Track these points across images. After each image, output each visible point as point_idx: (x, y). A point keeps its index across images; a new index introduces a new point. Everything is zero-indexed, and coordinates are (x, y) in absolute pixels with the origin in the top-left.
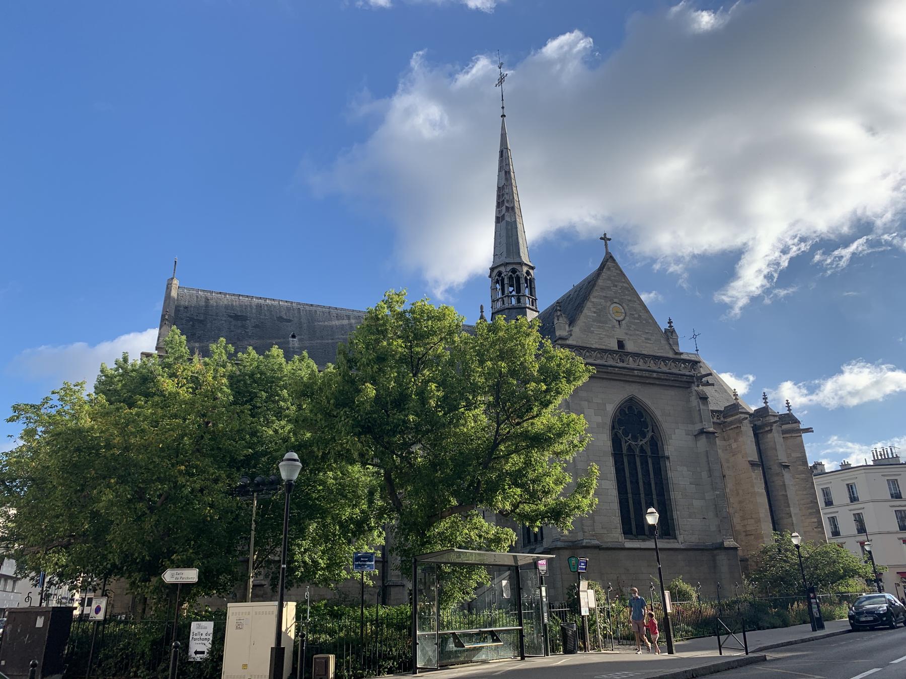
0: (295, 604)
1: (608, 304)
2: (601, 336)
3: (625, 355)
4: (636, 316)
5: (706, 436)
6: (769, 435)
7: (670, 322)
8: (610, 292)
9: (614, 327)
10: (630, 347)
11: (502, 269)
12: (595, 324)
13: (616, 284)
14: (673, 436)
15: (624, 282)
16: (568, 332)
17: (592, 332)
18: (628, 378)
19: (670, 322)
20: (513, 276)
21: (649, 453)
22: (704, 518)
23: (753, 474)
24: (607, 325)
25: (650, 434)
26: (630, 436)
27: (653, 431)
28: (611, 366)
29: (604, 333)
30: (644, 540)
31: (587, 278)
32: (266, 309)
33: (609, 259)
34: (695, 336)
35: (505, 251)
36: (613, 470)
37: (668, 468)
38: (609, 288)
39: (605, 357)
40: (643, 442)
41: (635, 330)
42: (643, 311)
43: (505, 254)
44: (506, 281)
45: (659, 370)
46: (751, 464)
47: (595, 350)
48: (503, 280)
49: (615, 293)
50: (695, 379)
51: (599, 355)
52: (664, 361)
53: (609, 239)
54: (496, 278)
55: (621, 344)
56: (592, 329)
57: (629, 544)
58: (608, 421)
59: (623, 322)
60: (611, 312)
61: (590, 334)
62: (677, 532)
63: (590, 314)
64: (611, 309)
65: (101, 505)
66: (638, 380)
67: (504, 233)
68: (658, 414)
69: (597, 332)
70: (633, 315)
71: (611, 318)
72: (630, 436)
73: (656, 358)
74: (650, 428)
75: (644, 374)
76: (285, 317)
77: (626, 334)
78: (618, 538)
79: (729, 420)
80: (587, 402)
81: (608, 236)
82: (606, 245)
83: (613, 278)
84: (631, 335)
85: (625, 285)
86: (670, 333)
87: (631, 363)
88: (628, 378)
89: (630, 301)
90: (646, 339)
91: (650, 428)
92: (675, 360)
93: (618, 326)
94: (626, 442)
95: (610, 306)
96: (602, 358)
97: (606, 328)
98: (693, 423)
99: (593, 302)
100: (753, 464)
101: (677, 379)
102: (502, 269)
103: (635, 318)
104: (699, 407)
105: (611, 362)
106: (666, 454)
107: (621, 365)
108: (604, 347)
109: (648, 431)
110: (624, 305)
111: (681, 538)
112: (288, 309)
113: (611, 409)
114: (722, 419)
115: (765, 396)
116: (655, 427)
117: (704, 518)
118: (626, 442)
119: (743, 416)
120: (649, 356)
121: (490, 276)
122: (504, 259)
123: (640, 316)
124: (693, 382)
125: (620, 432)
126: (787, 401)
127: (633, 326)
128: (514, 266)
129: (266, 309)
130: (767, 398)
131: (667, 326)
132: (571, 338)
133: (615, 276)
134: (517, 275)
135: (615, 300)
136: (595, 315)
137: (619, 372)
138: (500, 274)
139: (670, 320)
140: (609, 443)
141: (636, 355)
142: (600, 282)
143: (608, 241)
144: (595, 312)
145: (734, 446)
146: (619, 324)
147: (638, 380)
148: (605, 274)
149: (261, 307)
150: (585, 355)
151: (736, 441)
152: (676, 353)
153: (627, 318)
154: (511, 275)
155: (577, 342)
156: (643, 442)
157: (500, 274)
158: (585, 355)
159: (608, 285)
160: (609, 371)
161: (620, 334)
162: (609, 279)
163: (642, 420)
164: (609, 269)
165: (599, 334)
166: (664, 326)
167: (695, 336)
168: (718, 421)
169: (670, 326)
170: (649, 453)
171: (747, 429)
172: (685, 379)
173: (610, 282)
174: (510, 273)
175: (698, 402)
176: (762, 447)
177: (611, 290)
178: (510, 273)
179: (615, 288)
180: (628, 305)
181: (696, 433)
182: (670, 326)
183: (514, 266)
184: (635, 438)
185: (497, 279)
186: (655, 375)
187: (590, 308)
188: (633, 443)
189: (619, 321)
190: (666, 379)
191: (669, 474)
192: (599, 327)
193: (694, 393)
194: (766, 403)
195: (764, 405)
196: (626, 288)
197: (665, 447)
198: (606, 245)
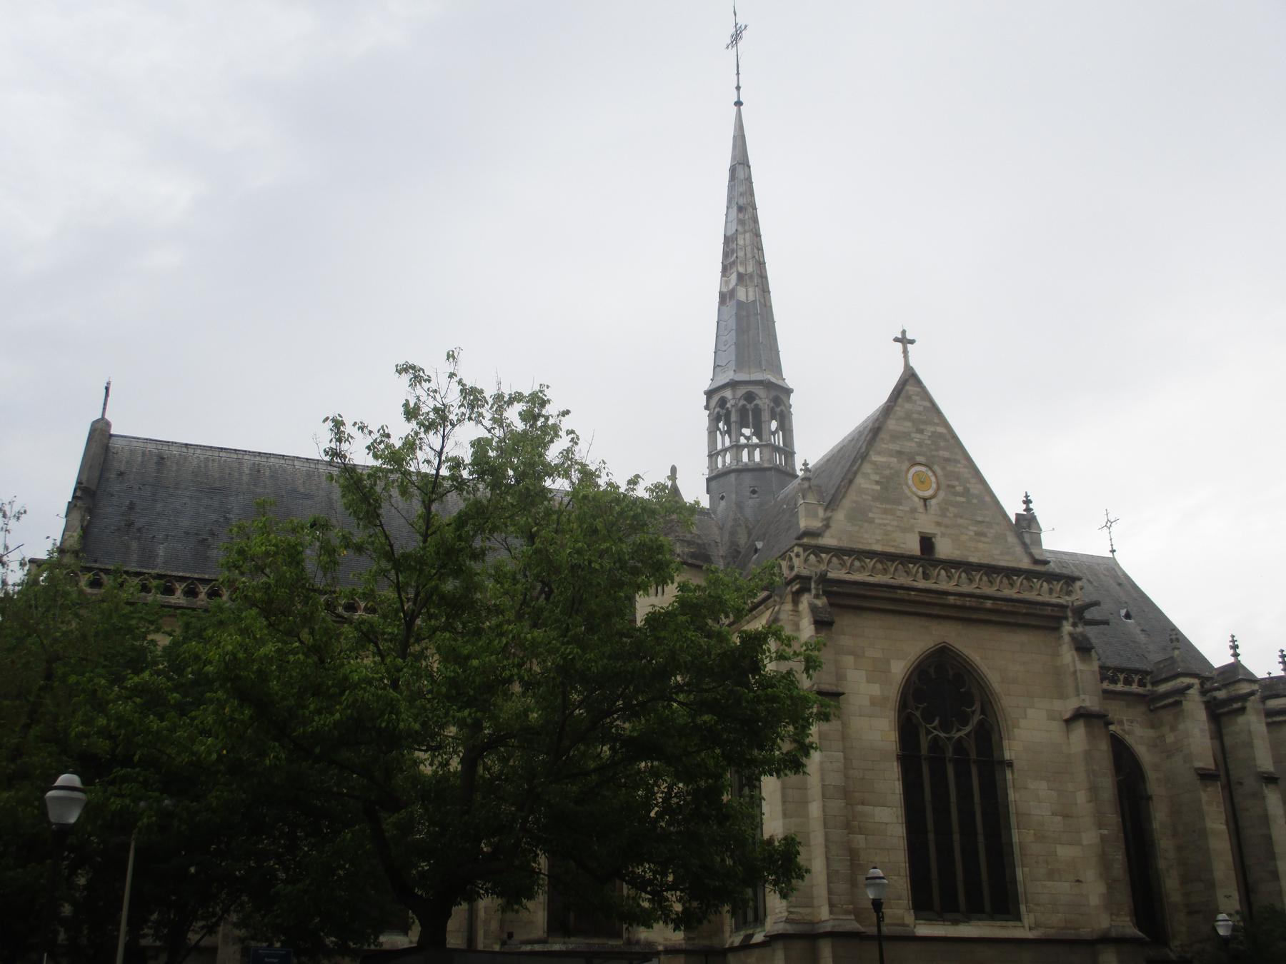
0: (140, 940)
1: (904, 467)
2: (889, 528)
3: (931, 566)
4: (959, 489)
5: (1087, 726)
6: (1241, 720)
7: (1027, 502)
8: (909, 444)
9: (914, 510)
10: (944, 549)
11: (728, 394)
12: (878, 504)
13: (922, 427)
14: (1023, 723)
15: (938, 425)
16: (823, 520)
17: (871, 521)
18: (936, 611)
19: (1027, 502)
20: (748, 406)
21: (973, 756)
22: (1078, 881)
23: (1202, 793)
24: (901, 508)
25: (977, 718)
26: (936, 722)
27: (983, 712)
28: (902, 587)
29: (895, 523)
30: (955, 922)
31: (872, 415)
32: (267, 474)
33: (909, 383)
34: (1109, 524)
35: (734, 357)
36: (898, 787)
37: (1010, 784)
38: (906, 436)
39: (892, 569)
40: (961, 734)
41: (956, 516)
42: (973, 481)
43: (733, 365)
44: (734, 418)
45: (999, 594)
46: (1199, 775)
47: (871, 554)
48: (728, 414)
49: (920, 444)
50: (1069, 614)
51: (879, 566)
52: (1008, 577)
53: (912, 342)
54: (717, 410)
55: (927, 543)
56: (870, 515)
57: (924, 930)
58: (893, 692)
59: (933, 502)
60: (910, 482)
61: (866, 525)
62: (1023, 908)
63: (869, 486)
64: (910, 475)
65: (992, 531)
66: (953, 613)
67: (732, 323)
68: (994, 679)
69: (880, 521)
70: (954, 487)
71: (909, 494)
72: (936, 722)
73: (991, 570)
74: (977, 706)
75: (968, 602)
76: (302, 490)
77: (938, 524)
78: (903, 918)
79: (1163, 688)
80: (852, 657)
81: (909, 336)
82: (905, 352)
83: (915, 416)
84: (947, 526)
85: (941, 430)
86: (1027, 523)
87: (943, 583)
88: (936, 611)
89: (947, 460)
90: (977, 534)
91: (977, 706)
92: (1029, 575)
93: (921, 509)
94: (928, 732)
95: (908, 470)
96: (885, 571)
97: (899, 513)
98: (1062, 696)
99: (874, 463)
100: (1205, 777)
101: (1030, 611)
102: (728, 394)
103: (956, 494)
104: (1075, 666)
105: (903, 580)
106: (1007, 756)
107: (922, 584)
108: (892, 550)
109: (973, 712)
110: (936, 468)
111: (1028, 919)
112: (309, 475)
113: (899, 669)
114: (1149, 687)
115: (1234, 641)
116: (988, 703)
117: (1078, 881)
118: (928, 732)
119: (1187, 680)
120: (979, 567)
121: (707, 407)
122: (728, 376)
123: (967, 490)
124: (1066, 618)
125: (918, 714)
126: (1282, 651)
127: (951, 509)
128: (751, 388)
129: (267, 474)
130: (1237, 647)
131: (1021, 509)
132: (827, 534)
133: (920, 413)
134: (757, 405)
135: (919, 459)
136: (878, 488)
137: (918, 598)
138: (723, 402)
139: (1027, 496)
140: (893, 736)
141: (952, 565)
142: (891, 424)
143: (909, 345)
144: (877, 483)
145: (1170, 738)
146: (925, 505)
147: (953, 613)
148: (898, 411)
149: (259, 471)
150: (852, 564)
151: (1173, 729)
152: (1036, 562)
153: (942, 494)
154: (744, 406)
155: (840, 539)
156: (961, 734)
157: (723, 402)
158: (852, 564)
159: (906, 430)
160: (898, 596)
161: (926, 523)
162: (908, 417)
163: (962, 690)
164: (909, 398)
165: (885, 525)
166: (1013, 508)
167: (1109, 524)
168: (1141, 690)
169: (1028, 510)
170: (973, 756)
171: (1195, 707)
172: (1048, 611)
173: (909, 424)
174: (742, 402)
175: (1073, 656)
176: (1228, 741)
177: (912, 440)
178: (742, 402)
179: (919, 436)
180: (943, 469)
181: (1067, 716)
182: (1028, 510)
183: (751, 388)
184: (945, 727)
185: (718, 413)
186: (989, 604)
187: (869, 474)
188: (942, 735)
189: (925, 500)
190: (1012, 613)
191: (1012, 795)
192: (885, 511)
193: (1067, 638)
194: (1236, 655)
195: (1232, 660)
196: (941, 436)
197: (1006, 743)
198: (905, 352)
